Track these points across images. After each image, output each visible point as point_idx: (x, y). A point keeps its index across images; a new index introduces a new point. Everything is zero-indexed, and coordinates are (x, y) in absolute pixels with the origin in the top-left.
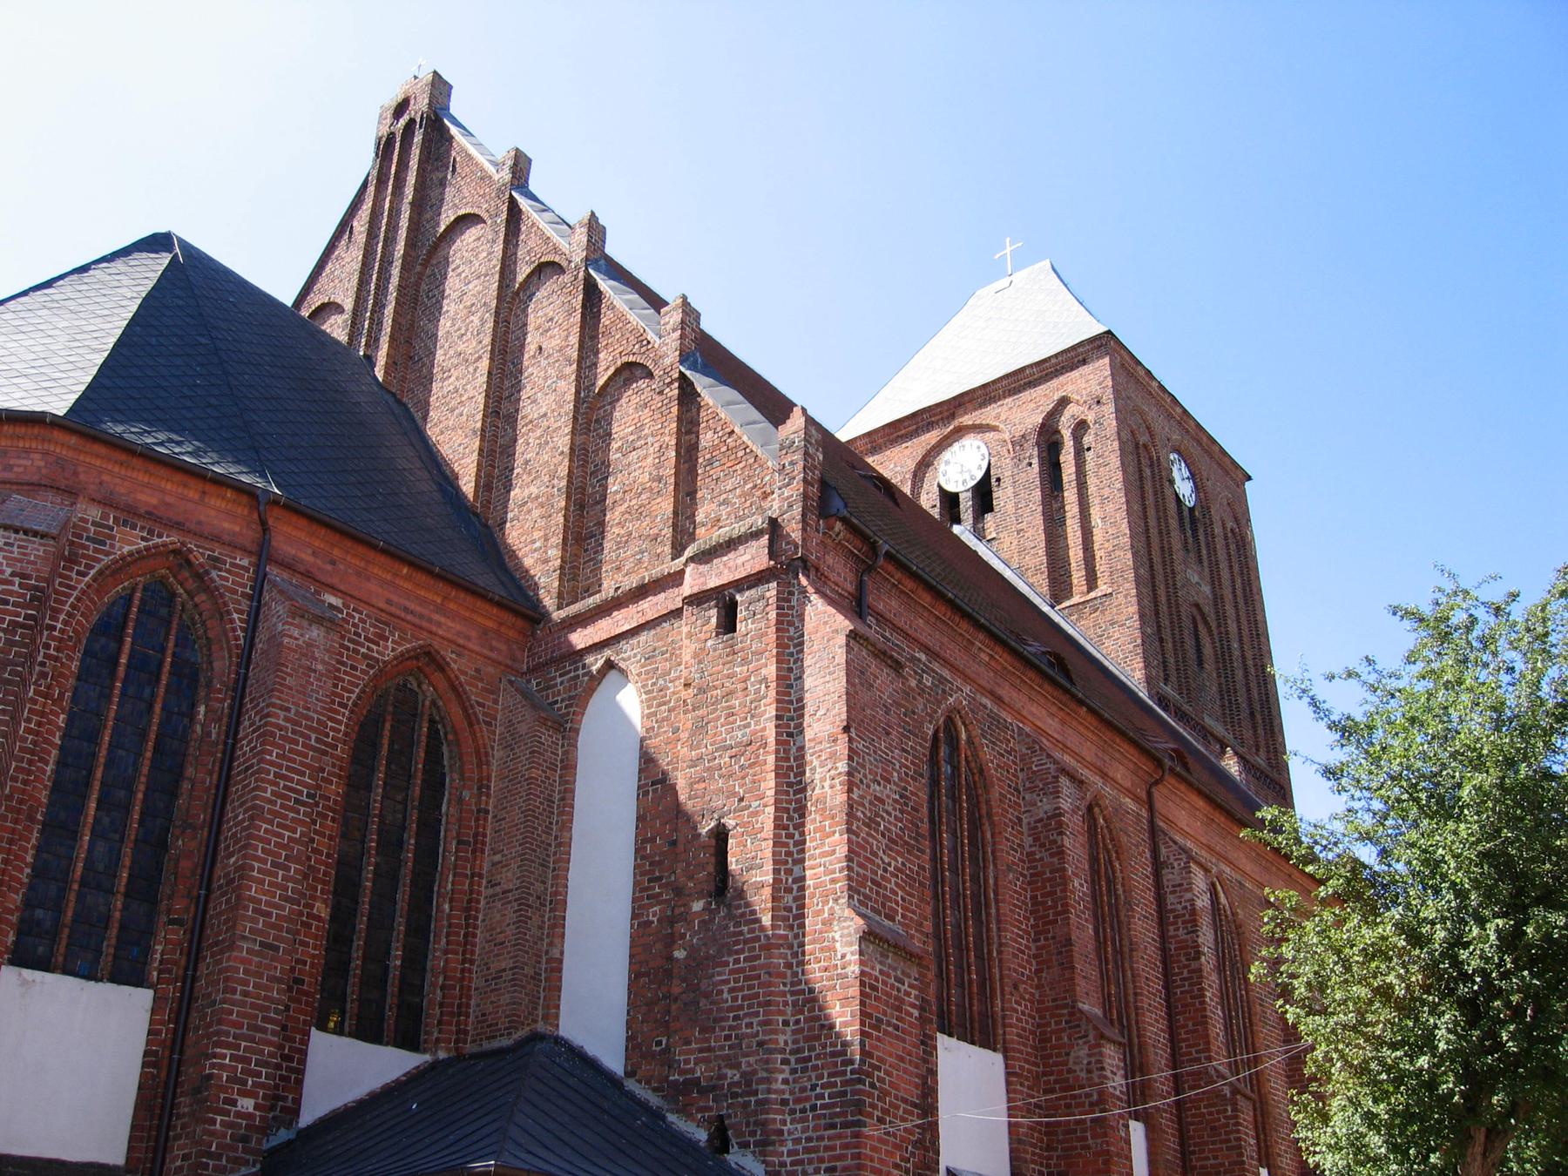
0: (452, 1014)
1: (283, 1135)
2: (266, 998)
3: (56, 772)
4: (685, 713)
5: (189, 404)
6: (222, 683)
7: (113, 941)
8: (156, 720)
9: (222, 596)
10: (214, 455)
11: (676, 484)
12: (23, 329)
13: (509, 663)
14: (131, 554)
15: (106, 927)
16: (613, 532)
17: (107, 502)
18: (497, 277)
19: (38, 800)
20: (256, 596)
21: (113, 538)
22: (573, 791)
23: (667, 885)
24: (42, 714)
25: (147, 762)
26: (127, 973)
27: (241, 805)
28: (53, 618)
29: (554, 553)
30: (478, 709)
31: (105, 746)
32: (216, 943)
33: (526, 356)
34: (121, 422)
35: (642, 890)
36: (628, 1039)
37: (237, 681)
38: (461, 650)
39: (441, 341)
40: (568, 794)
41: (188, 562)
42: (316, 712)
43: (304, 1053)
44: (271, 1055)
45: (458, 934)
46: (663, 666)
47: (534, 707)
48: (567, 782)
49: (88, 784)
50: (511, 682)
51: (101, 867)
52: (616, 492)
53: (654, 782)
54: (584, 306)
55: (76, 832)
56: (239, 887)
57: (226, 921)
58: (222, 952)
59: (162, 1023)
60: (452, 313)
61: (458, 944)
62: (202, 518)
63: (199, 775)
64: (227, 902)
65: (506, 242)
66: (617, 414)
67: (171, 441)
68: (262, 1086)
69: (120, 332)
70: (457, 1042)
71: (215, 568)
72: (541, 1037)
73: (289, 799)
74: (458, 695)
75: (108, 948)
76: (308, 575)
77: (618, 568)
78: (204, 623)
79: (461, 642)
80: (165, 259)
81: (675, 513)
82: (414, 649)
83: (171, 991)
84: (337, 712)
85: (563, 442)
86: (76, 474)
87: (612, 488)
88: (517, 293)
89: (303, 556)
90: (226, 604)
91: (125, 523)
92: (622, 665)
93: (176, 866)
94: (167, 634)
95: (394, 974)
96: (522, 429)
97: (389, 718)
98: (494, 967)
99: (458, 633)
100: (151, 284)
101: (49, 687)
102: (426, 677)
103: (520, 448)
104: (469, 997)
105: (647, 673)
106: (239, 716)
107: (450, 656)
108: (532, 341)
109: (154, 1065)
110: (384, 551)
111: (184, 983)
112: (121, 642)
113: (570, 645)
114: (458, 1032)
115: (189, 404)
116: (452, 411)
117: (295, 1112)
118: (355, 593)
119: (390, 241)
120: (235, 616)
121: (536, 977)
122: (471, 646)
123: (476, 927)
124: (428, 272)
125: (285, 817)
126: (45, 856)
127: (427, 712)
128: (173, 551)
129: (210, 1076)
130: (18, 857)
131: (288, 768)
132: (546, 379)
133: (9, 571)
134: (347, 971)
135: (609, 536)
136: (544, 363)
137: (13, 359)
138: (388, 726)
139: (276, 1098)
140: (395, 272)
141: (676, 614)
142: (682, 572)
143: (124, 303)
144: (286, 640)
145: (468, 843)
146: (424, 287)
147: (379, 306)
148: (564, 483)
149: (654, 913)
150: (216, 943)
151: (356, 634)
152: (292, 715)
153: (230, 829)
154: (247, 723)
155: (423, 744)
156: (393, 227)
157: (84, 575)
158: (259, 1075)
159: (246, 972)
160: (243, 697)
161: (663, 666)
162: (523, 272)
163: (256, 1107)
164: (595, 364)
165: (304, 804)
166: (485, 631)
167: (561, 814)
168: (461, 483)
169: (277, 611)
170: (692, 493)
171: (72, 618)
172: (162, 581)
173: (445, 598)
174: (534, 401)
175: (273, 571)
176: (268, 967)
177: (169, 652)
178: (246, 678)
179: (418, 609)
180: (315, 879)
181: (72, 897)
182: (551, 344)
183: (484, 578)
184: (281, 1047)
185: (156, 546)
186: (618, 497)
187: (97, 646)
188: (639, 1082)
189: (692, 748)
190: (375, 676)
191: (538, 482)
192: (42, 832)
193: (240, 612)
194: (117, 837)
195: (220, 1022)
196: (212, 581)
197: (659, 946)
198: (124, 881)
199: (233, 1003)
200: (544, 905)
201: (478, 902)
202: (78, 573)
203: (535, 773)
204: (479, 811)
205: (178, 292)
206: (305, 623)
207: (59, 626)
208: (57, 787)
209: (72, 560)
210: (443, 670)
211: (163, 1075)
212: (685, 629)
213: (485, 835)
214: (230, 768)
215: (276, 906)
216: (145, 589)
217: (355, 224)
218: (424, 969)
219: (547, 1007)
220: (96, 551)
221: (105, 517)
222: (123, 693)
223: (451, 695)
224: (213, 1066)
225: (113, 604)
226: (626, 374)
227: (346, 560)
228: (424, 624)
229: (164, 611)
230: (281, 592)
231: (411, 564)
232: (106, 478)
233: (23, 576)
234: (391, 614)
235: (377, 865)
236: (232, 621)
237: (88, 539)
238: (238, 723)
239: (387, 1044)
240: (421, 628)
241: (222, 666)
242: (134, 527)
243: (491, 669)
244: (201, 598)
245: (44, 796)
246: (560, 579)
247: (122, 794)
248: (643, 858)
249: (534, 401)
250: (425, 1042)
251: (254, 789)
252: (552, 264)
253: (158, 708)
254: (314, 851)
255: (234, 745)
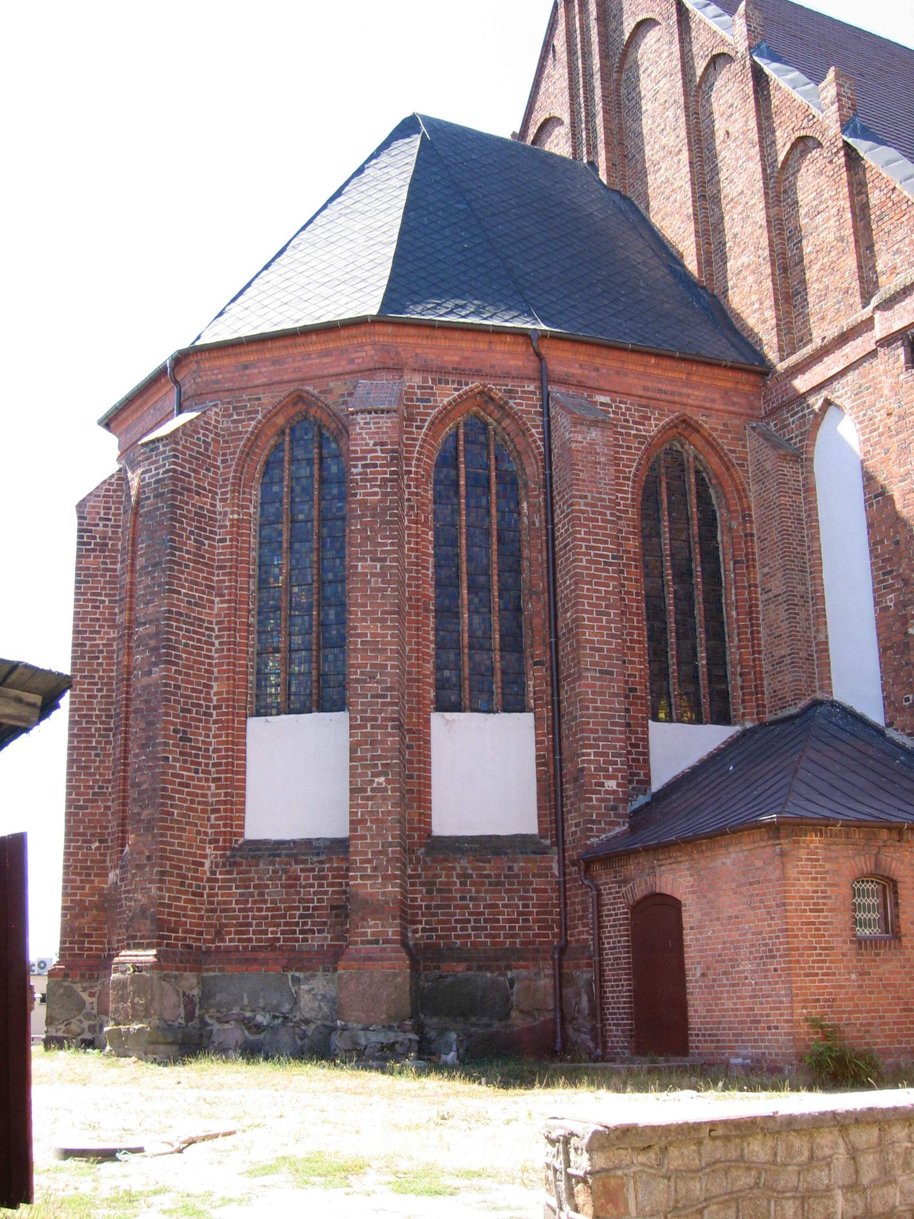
0: (751, 694)
1: (642, 800)
2: (611, 709)
3: (435, 573)
4: (890, 437)
5: (463, 268)
6: (535, 483)
7: (500, 684)
8: (494, 521)
9: (521, 418)
10: (491, 308)
11: (856, 241)
12: (331, 240)
13: (750, 412)
14: (450, 404)
15: (492, 675)
16: (814, 288)
17: (424, 369)
18: (680, 75)
19: (427, 596)
20: (545, 412)
21: (434, 395)
22: (816, 509)
23: (898, 575)
24: (418, 536)
25: (495, 553)
26: (514, 704)
27: (566, 574)
28: (408, 465)
29: (770, 314)
30: (731, 455)
31: (464, 548)
32: (569, 676)
33: (718, 142)
34: (419, 303)
35: (878, 583)
36: (885, 698)
37: (545, 480)
38: (708, 411)
39: (647, 139)
40: (812, 510)
41: (492, 399)
42: (606, 494)
43: (646, 740)
44: (621, 748)
45: (746, 633)
46: (869, 399)
47: (775, 447)
48: (810, 502)
49: (458, 577)
50: (753, 428)
51: (480, 634)
52: (810, 253)
53: (877, 496)
54: (756, 92)
55: (458, 613)
56: (577, 634)
57: (573, 659)
58: (574, 681)
59: (543, 735)
60: (650, 112)
61: (747, 640)
62: (494, 362)
63: (533, 555)
64: (571, 645)
65: (682, 41)
66: (799, 184)
67: (457, 306)
68: (619, 770)
69: (399, 221)
70: (758, 713)
71: (511, 398)
72: (821, 703)
73: (599, 563)
74: (713, 448)
75: (497, 689)
76: (580, 385)
77: (823, 318)
78: (512, 441)
79: (708, 405)
80: (414, 142)
81: (860, 267)
82: (672, 421)
83: (545, 712)
84: (623, 485)
85: (760, 216)
86: (397, 353)
87: (807, 250)
88: (699, 86)
89: (574, 371)
90: (525, 424)
91: (440, 382)
92: (837, 402)
93: (531, 623)
94: (489, 455)
95: (703, 671)
96: (726, 207)
97: (664, 478)
98: (777, 654)
99: (705, 399)
100: (411, 168)
101: (417, 515)
102: (686, 438)
103: (727, 223)
104: (762, 679)
105: (858, 406)
106: (552, 505)
107: (701, 419)
108: (720, 126)
109: (544, 764)
110: (633, 351)
111: (553, 705)
112: (457, 468)
113: (795, 390)
114: (758, 706)
115: (463, 268)
116: (668, 198)
117: (647, 782)
118: (618, 389)
119: (587, 55)
120: (533, 431)
121: (809, 658)
122: (716, 406)
123: (758, 625)
124: (624, 77)
125: (599, 577)
126: (442, 633)
127: (692, 465)
128: (479, 393)
129: (582, 769)
130: (424, 639)
131: (595, 541)
132: (737, 160)
133: (372, 442)
134: (667, 675)
135: (811, 292)
136: (733, 145)
137: (332, 269)
138: (664, 485)
139: (632, 774)
140: (597, 83)
141: (873, 354)
142: (871, 319)
143: (396, 193)
144: (574, 445)
145: (742, 562)
146: (623, 91)
147: (591, 116)
148: (767, 253)
149: (890, 600)
150: (569, 676)
151: (625, 421)
152: (589, 500)
153: (562, 592)
154: (558, 511)
155: (694, 491)
156: (586, 43)
157: (421, 427)
158: (616, 763)
159: (594, 693)
160: (552, 492)
161: (869, 399)
162: (700, 66)
163: (618, 785)
164: (774, 142)
165: (611, 564)
166: (726, 392)
167: (810, 528)
168: (686, 263)
169: (562, 421)
170: (870, 247)
171: (421, 463)
172: (476, 416)
173: (689, 374)
174: (732, 181)
175: (553, 389)
176: (608, 687)
177: (493, 468)
178: (551, 477)
179: (669, 388)
180: (631, 614)
181: (466, 659)
182: (736, 128)
183: (718, 347)
184: (629, 738)
185: (466, 393)
186: (812, 257)
187: (442, 476)
188: (896, 730)
189: (900, 465)
190: (646, 449)
191: (747, 252)
192: (435, 617)
193: (536, 427)
194: (486, 610)
195: (582, 731)
196: (511, 408)
197: (898, 625)
198: (498, 640)
199: (588, 717)
200: (808, 603)
201: (757, 606)
202: (418, 427)
203: (783, 500)
204: (746, 535)
205: (433, 169)
206: (585, 429)
207: (413, 469)
208: (438, 584)
209: (410, 419)
210: (698, 431)
211: (552, 771)
212: (882, 367)
213: (753, 554)
214: (554, 547)
215: (606, 643)
216: (465, 425)
217: (555, 42)
218: (725, 663)
219: (821, 679)
220: (425, 407)
221: (425, 380)
222: (468, 506)
223: (707, 448)
224: (583, 762)
225: (446, 442)
226: (801, 147)
227: (608, 362)
228: (677, 399)
229: (482, 438)
230: (563, 407)
231: (657, 355)
232: (419, 351)
233: (382, 444)
234: (648, 398)
235: (675, 592)
236: (532, 435)
237: (418, 400)
238: (552, 512)
239: (706, 723)
240: (674, 403)
241: (532, 470)
242: (447, 383)
243: (736, 422)
244: (506, 422)
245: (431, 593)
246: (778, 335)
247: (482, 579)
248: (876, 557)
249: (732, 181)
250: (735, 716)
251: (573, 561)
252: (723, 54)
253: (494, 511)
254: (627, 593)
255: (553, 529)
